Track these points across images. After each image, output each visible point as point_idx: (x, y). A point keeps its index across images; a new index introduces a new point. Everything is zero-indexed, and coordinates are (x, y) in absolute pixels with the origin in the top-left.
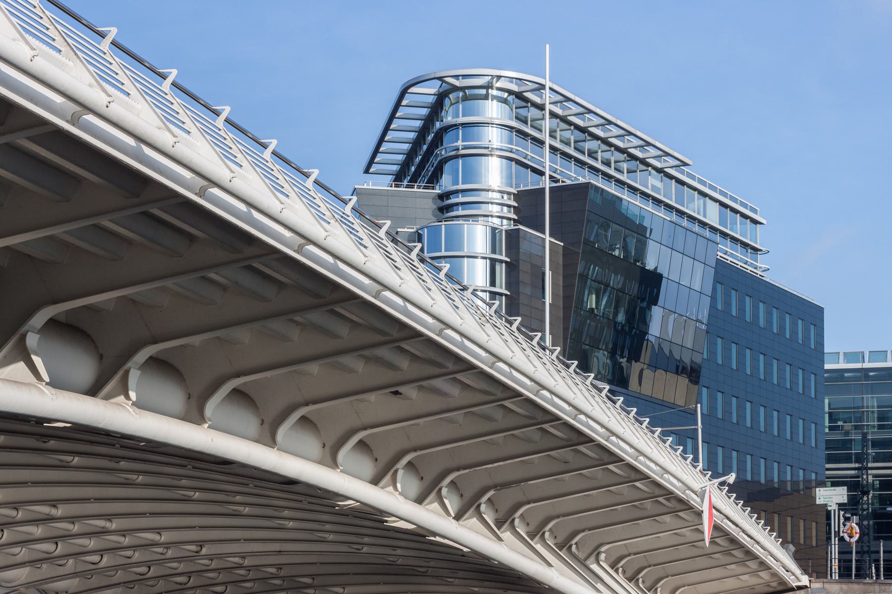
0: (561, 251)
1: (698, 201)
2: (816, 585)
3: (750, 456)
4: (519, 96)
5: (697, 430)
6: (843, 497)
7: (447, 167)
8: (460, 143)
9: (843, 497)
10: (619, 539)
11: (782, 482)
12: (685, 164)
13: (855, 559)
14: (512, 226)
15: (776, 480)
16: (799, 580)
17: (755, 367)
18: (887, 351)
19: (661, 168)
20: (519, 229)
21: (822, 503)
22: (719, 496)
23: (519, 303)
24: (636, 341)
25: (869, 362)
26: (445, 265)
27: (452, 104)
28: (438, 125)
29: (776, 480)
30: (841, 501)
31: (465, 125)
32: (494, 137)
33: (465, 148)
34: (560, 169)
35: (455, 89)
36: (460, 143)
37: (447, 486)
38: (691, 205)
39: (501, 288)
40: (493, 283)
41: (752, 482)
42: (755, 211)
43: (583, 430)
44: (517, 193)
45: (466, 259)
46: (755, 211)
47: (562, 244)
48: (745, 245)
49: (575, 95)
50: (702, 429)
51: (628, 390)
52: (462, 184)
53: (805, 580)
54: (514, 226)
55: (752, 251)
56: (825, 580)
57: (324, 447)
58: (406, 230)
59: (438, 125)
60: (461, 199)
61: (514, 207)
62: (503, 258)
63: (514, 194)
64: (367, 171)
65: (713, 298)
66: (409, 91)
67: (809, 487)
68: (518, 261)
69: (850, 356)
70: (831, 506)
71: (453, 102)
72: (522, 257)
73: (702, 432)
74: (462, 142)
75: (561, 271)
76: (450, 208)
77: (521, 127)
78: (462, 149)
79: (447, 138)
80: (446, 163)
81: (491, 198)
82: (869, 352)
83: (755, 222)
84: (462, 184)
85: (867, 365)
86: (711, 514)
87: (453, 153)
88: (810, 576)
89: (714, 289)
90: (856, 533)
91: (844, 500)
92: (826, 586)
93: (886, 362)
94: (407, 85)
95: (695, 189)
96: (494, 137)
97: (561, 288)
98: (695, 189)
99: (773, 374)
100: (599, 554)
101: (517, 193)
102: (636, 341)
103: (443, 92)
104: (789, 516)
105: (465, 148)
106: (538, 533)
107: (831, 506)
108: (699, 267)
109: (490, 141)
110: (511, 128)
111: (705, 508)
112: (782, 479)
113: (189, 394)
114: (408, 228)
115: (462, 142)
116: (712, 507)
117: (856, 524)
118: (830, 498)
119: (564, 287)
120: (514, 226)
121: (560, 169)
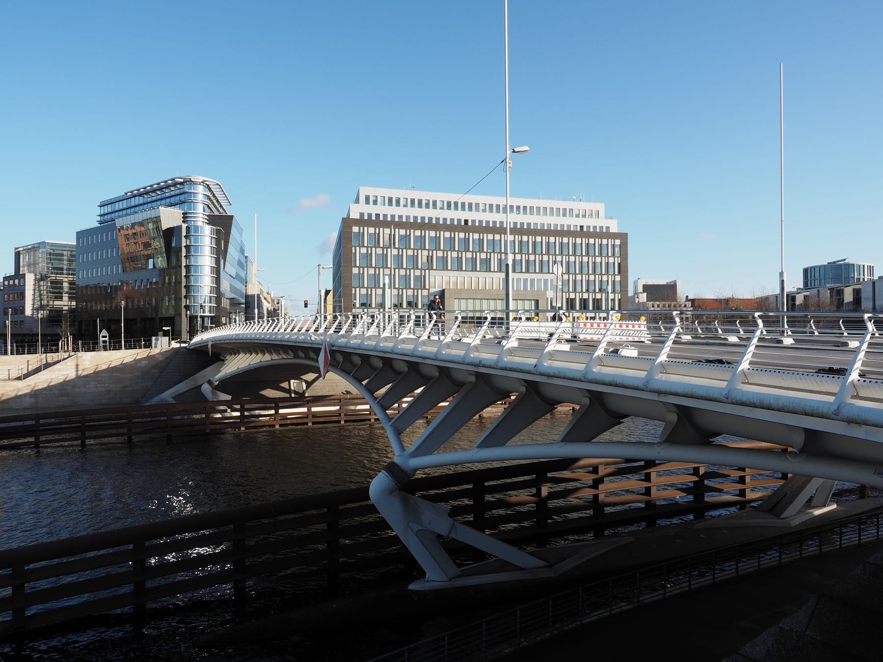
32: (200, 197)
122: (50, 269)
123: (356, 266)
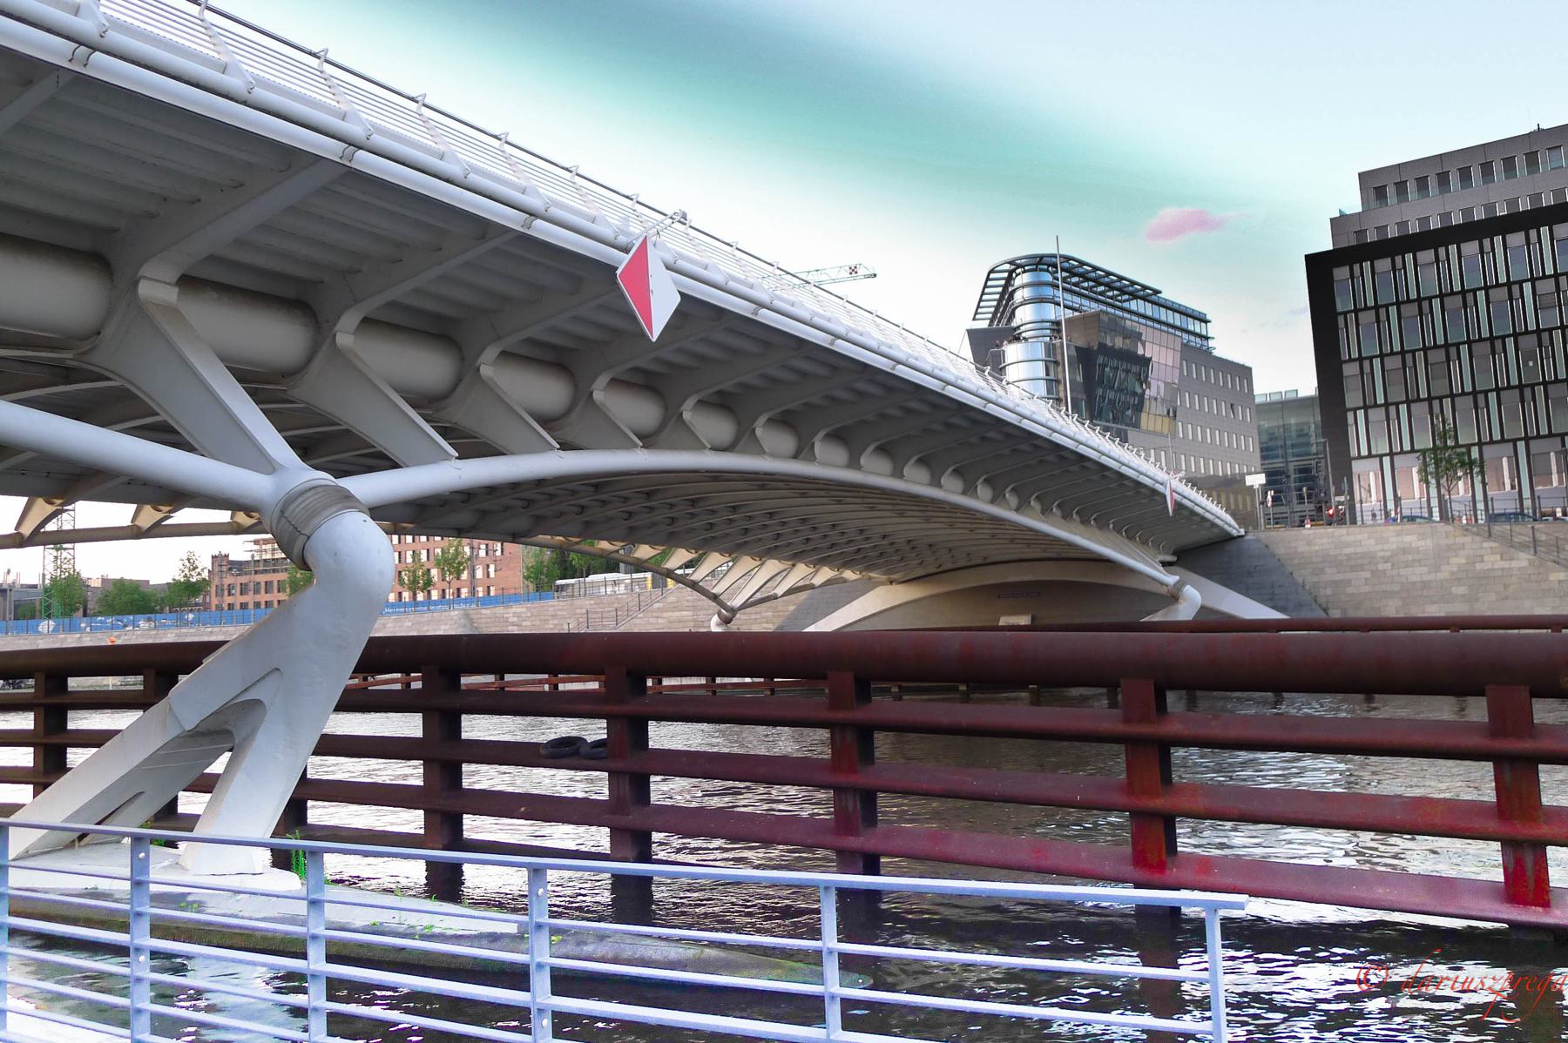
10: (697, 227)
15: (1229, 473)
16: (1239, 532)
22: (910, 503)
24: (926, 916)
28: (1010, 289)
29: (1229, 473)
37: (1034, 500)
40: (1047, 374)
41: (1214, 475)
43: (964, 889)
51: (1165, 382)
59: (1010, 289)
65: (1181, 369)
67: (1243, 476)
86: (1172, 495)
89: (1181, 364)
91: (1264, 482)
102: (926, 916)
108: (1171, 353)
111: (1168, 494)
116: (1173, 491)
122: (1531, 364)
123: (1351, 360)
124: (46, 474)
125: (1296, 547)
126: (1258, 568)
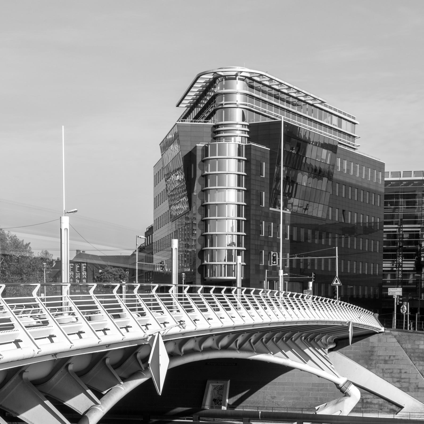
0: (269, 153)
1: (329, 117)
2: (388, 331)
3: (338, 184)
4: (250, 78)
5: (335, 258)
6: (400, 293)
7: (217, 112)
8: (223, 102)
9: (400, 293)
11: (358, 223)
12: (324, 102)
13: (405, 321)
14: (247, 143)
17: (353, 195)
18: (412, 171)
19: (312, 104)
20: (251, 145)
21: (391, 295)
23: (251, 179)
25: (403, 177)
26: (269, 290)
27: (220, 82)
30: (399, 294)
31: (225, 94)
32: (239, 99)
33: (226, 104)
34: (268, 111)
35: (221, 76)
36: (223, 102)
38: (326, 120)
39: (243, 172)
42: (354, 118)
44: (249, 124)
45: (227, 160)
46: (354, 118)
47: (269, 149)
48: (349, 135)
49: (276, 77)
50: (338, 258)
52: (224, 121)
53: (383, 329)
54: (248, 143)
55: (353, 137)
56: (391, 329)
57: (213, 340)
58: (200, 145)
60: (224, 128)
61: (248, 131)
62: (244, 158)
63: (248, 125)
64: (178, 106)
66: (200, 77)
68: (250, 159)
69: (394, 174)
70: (395, 296)
71: (220, 81)
72: (252, 157)
73: (338, 259)
74: (225, 101)
75: (269, 162)
76: (219, 132)
77: (251, 93)
78: (225, 105)
79: (217, 99)
80: (217, 110)
81: (237, 128)
82: (403, 172)
83: (355, 124)
84: (224, 121)
85: (402, 179)
87: (220, 107)
88: (385, 327)
90: (405, 310)
91: (401, 294)
92: (392, 332)
93: (411, 177)
94: (199, 76)
95: (327, 112)
96: (239, 99)
97: (269, 170)
98: (327, 112)
99: (361, 198)
100: (302, 337)
101: (249, 124)
103: (215, 77)
104: (361, 238)
105: (226, 104)
106: (281, 338)
107: (395, 296)
109: (237, 101)
110: (247, 94)
112: (364, 222)
113: (175, 343)
114: (201, 144)
115: (225, 101)
117: (406, 305)
118: (394, 293)
119: (270, 169)
120: (248, 143)
121: (268, 111)
124: (399, 371)
125: (418, 345)
126: (392, 358)
